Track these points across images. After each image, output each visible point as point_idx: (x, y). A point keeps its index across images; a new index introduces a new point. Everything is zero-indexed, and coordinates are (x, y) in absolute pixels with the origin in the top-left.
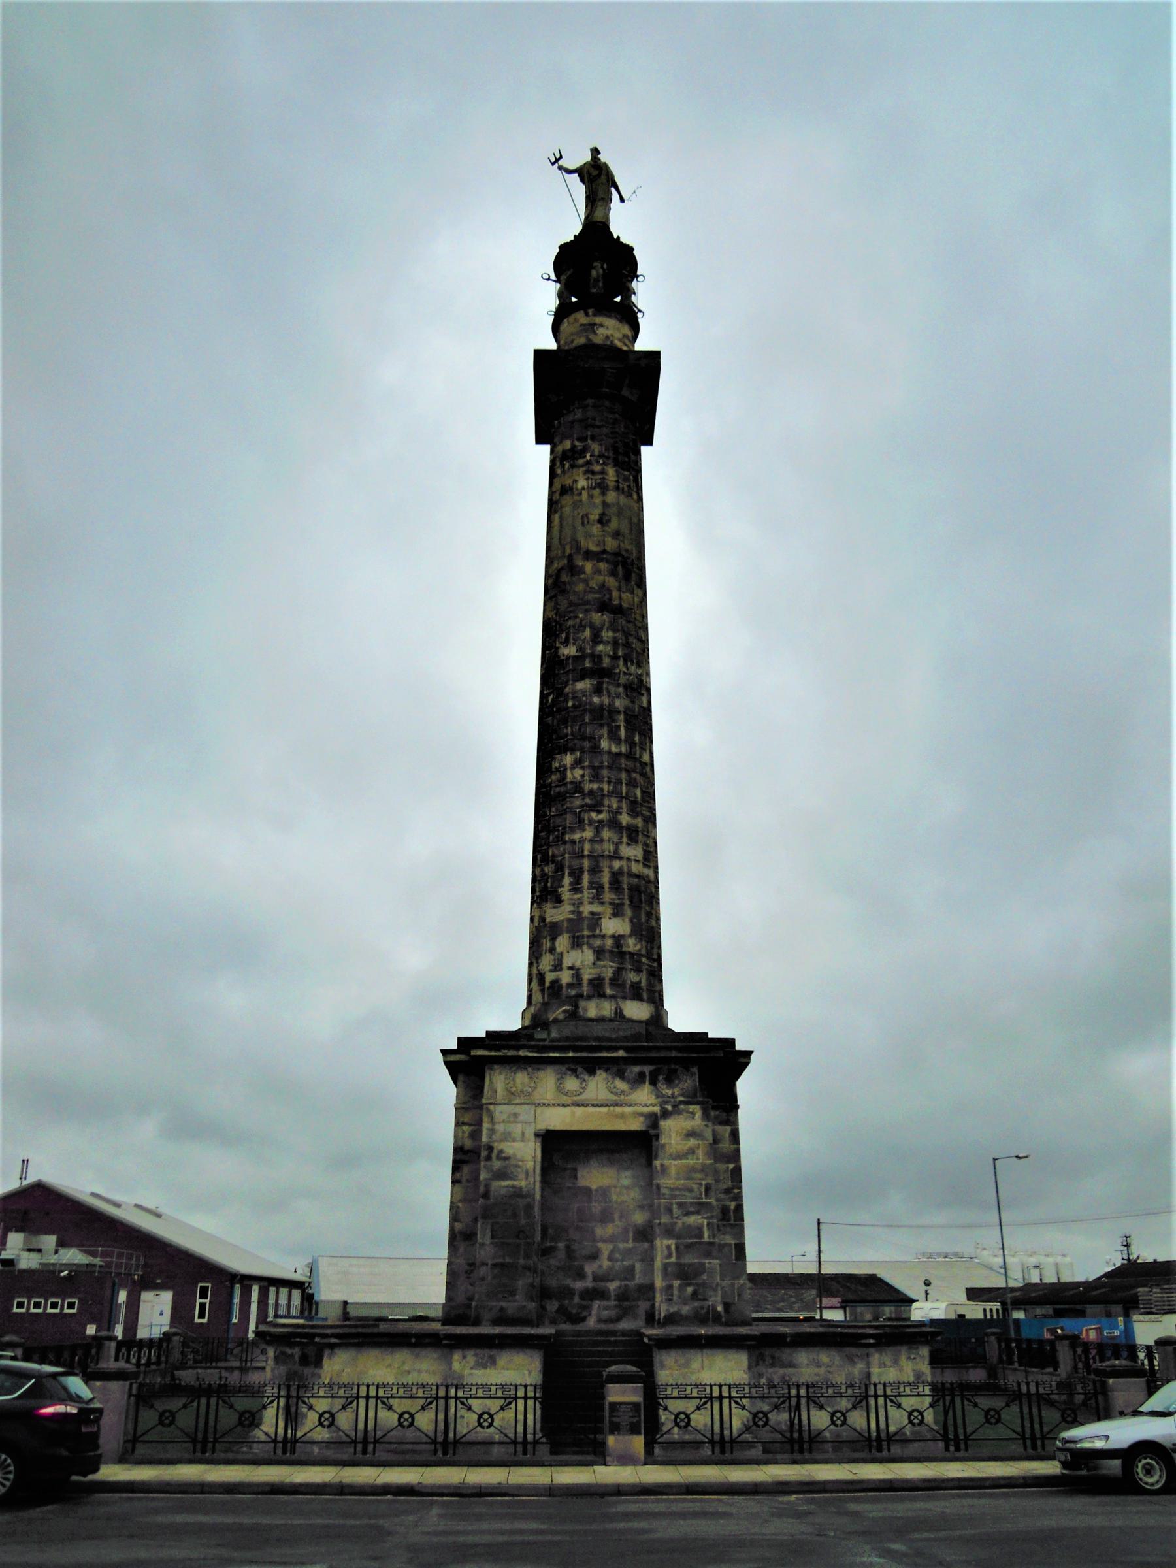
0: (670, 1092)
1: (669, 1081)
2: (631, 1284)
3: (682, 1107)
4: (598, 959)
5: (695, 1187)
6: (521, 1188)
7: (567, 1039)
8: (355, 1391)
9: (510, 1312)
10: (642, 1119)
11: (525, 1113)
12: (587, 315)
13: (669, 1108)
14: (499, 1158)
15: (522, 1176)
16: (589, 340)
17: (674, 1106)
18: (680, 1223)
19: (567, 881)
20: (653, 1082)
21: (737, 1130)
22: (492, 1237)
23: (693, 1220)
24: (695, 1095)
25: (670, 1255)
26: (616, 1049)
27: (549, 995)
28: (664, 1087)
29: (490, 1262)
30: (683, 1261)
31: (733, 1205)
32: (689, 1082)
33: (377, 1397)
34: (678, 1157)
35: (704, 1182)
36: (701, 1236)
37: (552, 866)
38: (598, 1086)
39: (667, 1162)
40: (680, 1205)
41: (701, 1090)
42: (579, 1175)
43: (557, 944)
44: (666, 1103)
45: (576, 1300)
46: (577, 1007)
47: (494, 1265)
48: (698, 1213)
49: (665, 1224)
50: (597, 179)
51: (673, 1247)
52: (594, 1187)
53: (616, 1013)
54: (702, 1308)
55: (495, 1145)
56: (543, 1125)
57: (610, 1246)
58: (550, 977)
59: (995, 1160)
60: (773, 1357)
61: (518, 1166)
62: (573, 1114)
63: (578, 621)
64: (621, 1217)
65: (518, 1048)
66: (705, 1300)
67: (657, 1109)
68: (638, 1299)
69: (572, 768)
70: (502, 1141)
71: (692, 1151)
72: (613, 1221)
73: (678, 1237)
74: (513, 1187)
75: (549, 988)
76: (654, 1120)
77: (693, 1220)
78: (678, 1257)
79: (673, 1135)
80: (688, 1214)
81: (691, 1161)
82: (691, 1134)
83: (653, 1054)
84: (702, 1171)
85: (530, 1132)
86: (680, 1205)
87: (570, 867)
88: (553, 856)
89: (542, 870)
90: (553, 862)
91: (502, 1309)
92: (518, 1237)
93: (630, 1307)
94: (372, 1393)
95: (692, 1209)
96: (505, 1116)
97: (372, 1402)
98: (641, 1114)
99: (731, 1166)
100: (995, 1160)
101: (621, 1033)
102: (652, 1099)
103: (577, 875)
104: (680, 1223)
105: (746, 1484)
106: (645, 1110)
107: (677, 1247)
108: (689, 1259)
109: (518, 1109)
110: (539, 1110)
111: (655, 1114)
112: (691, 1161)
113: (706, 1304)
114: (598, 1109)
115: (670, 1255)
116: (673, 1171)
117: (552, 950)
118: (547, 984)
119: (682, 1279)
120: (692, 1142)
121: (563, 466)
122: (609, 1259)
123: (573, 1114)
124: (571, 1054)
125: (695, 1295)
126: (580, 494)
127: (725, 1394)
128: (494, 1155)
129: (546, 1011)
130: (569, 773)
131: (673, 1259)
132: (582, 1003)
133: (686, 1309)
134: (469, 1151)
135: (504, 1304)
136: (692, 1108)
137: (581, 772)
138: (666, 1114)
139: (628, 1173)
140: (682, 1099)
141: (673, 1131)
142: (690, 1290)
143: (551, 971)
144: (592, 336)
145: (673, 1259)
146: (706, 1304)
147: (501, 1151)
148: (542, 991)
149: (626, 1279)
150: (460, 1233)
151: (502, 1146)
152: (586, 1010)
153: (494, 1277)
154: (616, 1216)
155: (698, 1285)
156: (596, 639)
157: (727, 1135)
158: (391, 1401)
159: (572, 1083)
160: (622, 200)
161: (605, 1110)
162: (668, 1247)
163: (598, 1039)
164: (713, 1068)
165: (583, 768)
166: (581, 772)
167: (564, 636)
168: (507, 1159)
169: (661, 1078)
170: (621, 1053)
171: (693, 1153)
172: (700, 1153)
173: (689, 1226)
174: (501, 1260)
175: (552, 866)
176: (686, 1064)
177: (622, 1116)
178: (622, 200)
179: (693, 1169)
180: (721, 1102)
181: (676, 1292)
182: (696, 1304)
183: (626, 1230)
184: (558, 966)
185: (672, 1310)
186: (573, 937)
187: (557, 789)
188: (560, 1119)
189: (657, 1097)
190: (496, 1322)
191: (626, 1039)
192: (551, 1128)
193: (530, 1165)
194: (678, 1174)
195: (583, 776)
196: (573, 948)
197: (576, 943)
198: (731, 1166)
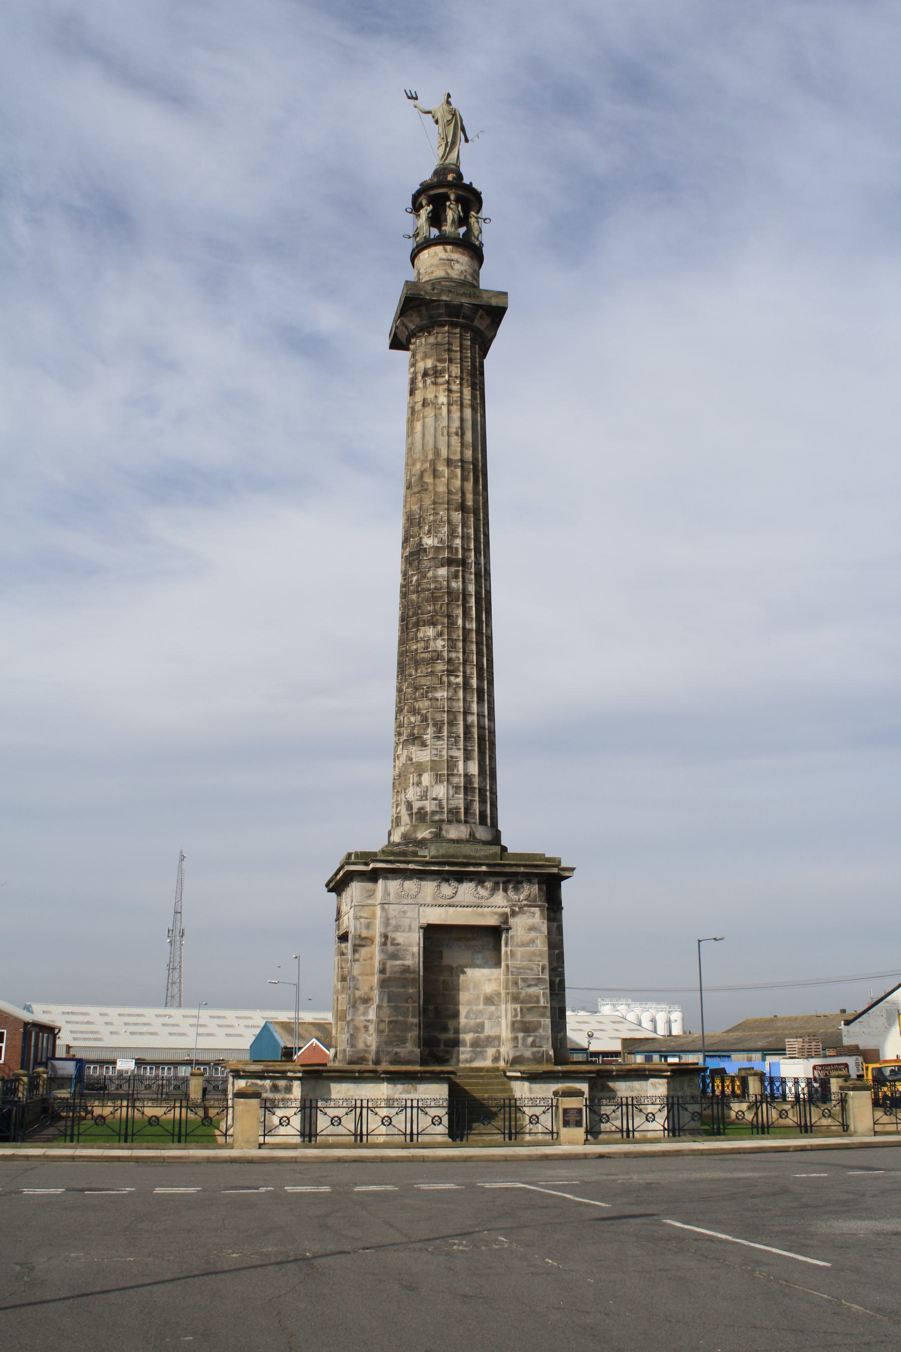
0: (516, 897)
1: (516, 889)
2: (482, 1036)
3: (525, 908)
4: (456, 793)
5: (535, 967)
6: (409, 966)
7: (443, 856)
8: (404, 1103)
9: (402, 1055)
10: (496, 917)
11: (411, 912)
12: (446, 251)
13: (517, 909)
14: (392, 944)
15: (409, 957)
16: (447, 273)
17: (520, 908)
18: (523, 992)
19: (430, 730)
20: (505, 890)
21: (561, 925)
22: (389, 1002)
23: (533, 990)
24: (535, 901)
25: (516, 1016)
26: (481, 865)
27: (416, 819)
28: (513, 893)
29: (387, 1020)
30: (526, 1019)
31: (557, 980)
32: (530, 890)
33: (418, 1107)
34: (523, 945)
35: (541, 964)
36: (538, 1001)
37: (419, 718)
38: (467, 891)
39: (514, 949)
40: (524, 980)
41: (540, 896)
42: (444, 955)
43: (423, 778)
44: (515, 905)
45: (442, 1047)
46: (441, 829)
47: (390, 1022)
48: (536, 985)
49: (513, 993)
50: (455, 128)
51: (519, 1009)
52: (455, 965)
53: (470, 835)
54: (539, 1052)
55: (390, 934)
56: (424, 921)
57: (467, 1008)
58: (416, 805)
59: (699, 941)
60: (602, 1085)
61: (407, 950)
62: (447, 912)
63: (439, 517)
64: (474, 988)
65: (408, 862)
66: (541, 1047)
67: (508, 910)
68: (487, 1046)
69: (435, 639)
70: (394, 931)
71: (533, 941)
72: (469, 990)
73: (522, 1002)
74: (403, 965)
75: (416, 813)
76: (505, 918)
77: (533, 990)
78: (522, 1017)
79: (519, 929)
80: (529, 986)
81: (531, 948)
82: (532, 929)
83: (507, 870)
84: (540, 955)
85: (415, 926)
86: (524, 980)
87: (433, 719)
88: (419, 709)
89: (409, 719)
90: (419, 713)
91: (396, 1053)
92: (407, 1002)
93: (481, 1052)
94: (415, 1104)
95: (533, 983)
96: (395, 913)
97: (415, 1110)
98: (496, 913)
99: (557, 952)
100: (699, 941)
101: (482, 853)
102: (505, 903)
103: (439, 726)
104: (523, 992)
105: (659, 1152)
106: (500, 910)
107: (521, 1010)
108: (529, 1018)
109: (406, 908)
110: (422, 909)
111: (507, 914)
112: (531, 948)
113: (541, 1049)
114: (465, 909)
115: (516, 1016)
116: (519, 956)
117: (419, 784)
118: (415, 810)
119: (525, 1032)
120: (533, 934)
121: (425, 382)
122: (466, 1017)
123: (447, 912)
124: (447, 868)
125: (533, 1045)
126: (441, 408)
127: (630, 1102)
128: (389, 943)
129: (415, 831)
130: (432, 643)
131: (519, 1018)
132: (445, 827)
133: (528, 1054)
134: (366, 938)
135: (398, 1050)
136: (533, 909)
137: (442, 643)
138: (514, 913)
139: (480, 956)
140: (525, 902)
141: (519, 924)
142: (530, 1039)
143: (418, 800)
144: (449, 271)
145: (519, 1018)
146: (541, 1049)
147: (394, 939)
148: (411, 815)
149: (477, 1032)
150: (360, 998)
151: (394, 935)
152: (447, 832)
153: (390, 1031)
154: (471, 986)
155: (536, 1036)
156: (452, 534)
157: (554, 929)
158: (427, 1110)
159: (447, 889)
160: (467, 140)
161: (469, 909)
162: (515, 1010)
163: (465, 857)
164: (546, 881)
165: (443, 640)
166: (442, 643)
167: (427, 528)
168: (398, 944)
169: (510, 886)
170: (484, 868)
171: (534, 942)
172: (538, 942)
173: (530, 995)
174: (395, 1018)
175: (419, 718)
176: (528, 878)
177: (482, 915)
178: (467, 140)
179: (533, 954)
180: (553, 906)
181: (520, 1041)
182: (535, 1049)
183: (478, 998)
184: (424, 797)
185: (517, 1054)
186: (437, 775)
187: (422, 655)
188: (437, 916)
189: (508, 901)
190: (392, 1063)
191: (486, 857)
192: (431, 922)
193: (415, 949)
194: (522, 957)
195: (443, 646)
196: (436, 783)
197: (438, 779)
198: (557, 952)
